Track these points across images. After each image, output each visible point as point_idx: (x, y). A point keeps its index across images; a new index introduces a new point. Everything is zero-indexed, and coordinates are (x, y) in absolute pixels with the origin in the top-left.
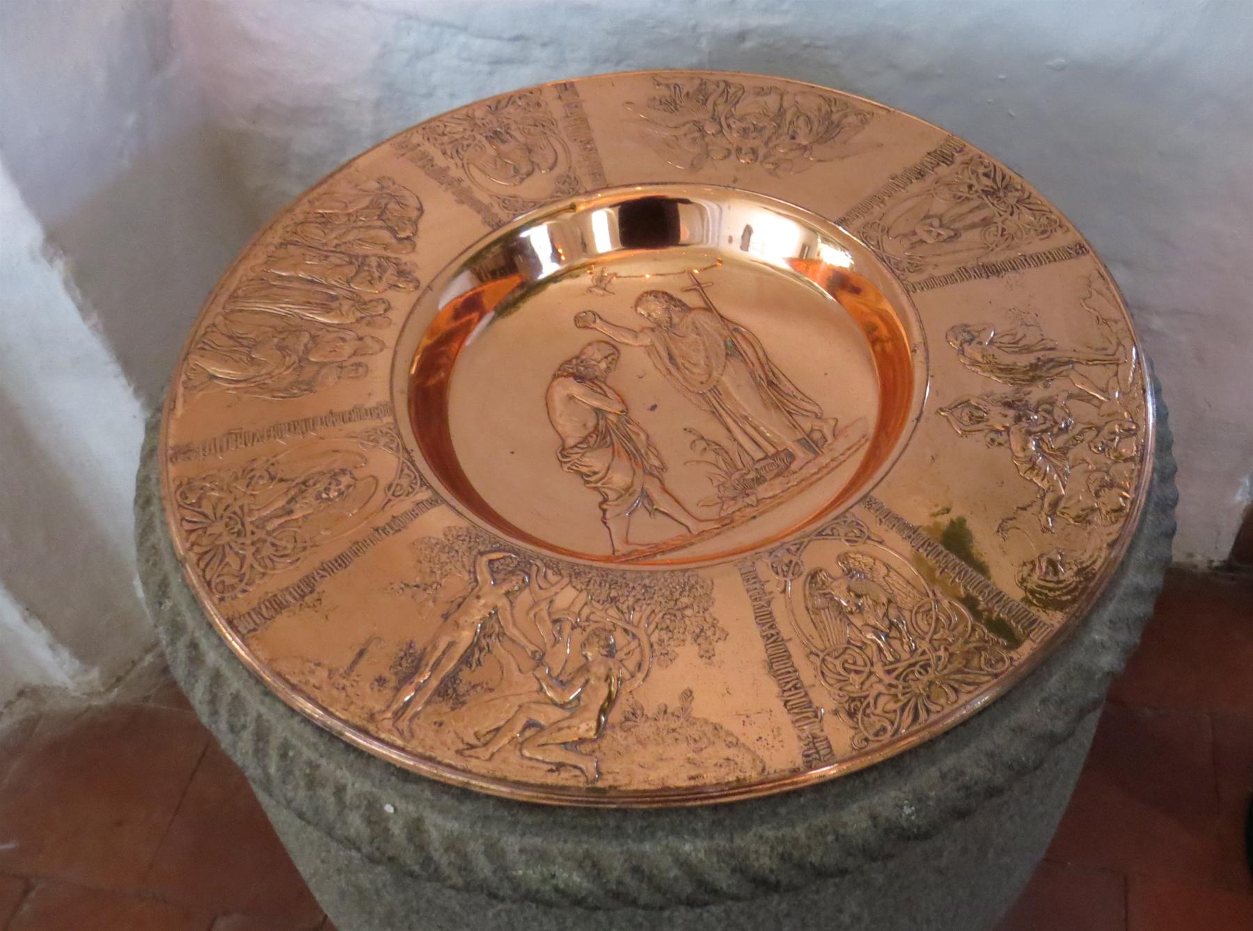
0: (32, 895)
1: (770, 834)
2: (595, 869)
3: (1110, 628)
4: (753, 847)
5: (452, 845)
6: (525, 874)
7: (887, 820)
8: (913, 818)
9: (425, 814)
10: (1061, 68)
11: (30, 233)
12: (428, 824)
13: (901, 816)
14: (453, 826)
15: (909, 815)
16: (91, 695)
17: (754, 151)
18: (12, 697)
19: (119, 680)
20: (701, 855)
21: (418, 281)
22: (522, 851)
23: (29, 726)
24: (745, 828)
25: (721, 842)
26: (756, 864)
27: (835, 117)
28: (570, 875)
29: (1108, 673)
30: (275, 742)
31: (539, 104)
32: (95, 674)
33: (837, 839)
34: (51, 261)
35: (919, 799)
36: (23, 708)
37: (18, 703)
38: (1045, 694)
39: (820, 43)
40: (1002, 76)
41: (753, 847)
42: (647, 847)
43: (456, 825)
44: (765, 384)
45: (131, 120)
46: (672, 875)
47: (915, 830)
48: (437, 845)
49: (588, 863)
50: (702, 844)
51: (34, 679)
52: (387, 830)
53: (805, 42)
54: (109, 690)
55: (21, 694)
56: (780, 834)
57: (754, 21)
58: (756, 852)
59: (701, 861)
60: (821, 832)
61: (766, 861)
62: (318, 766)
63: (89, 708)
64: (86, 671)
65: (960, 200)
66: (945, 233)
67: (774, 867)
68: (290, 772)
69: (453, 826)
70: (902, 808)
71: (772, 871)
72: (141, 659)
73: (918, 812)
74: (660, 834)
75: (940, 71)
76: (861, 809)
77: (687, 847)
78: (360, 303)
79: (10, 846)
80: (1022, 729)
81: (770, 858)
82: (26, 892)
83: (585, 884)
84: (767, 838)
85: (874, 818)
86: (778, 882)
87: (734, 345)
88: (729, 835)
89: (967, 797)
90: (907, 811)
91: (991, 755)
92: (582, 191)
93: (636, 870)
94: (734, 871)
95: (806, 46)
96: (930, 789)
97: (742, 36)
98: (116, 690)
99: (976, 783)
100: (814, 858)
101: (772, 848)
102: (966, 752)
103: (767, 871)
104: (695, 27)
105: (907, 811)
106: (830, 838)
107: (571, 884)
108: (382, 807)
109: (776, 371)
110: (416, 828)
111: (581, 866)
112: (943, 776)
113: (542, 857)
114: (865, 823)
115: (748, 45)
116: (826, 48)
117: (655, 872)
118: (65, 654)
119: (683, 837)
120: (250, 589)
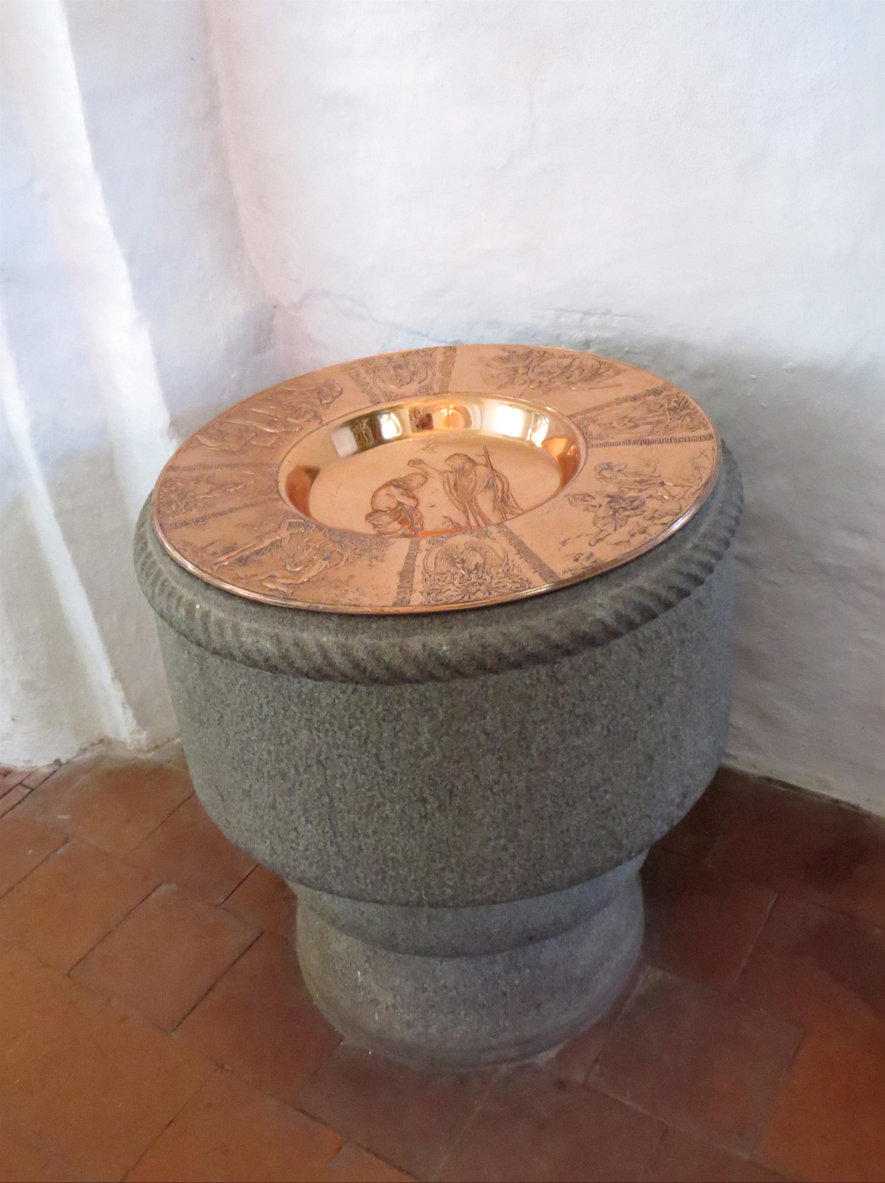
0: (67, 845)
1: (367, 641)
2: (277, 640)
3: (610, 600)
4: (357, 646)
5: (219, 623)
6: (246, 640)
7: (431, 648)
8: (447, 653)
9: (212, 610)
10: (793, 370)
11: (163, 419)
12: (212, 613)
13: (440, 650)
14: (222, 615)
15: (445, 651)
16: (140, 751)
17: (541, 382)
18: (96, 741)
19: (157, 747)
20: (330, 644)
21: (322, 421)
22: (248, 629)
23: (99, 759)
24: (354, 633)
25: (341, 639)
26: (355, 654)
27: (601, 371)
28: (266, 643)
29: (599, 620)
30: (162, 579)
31: (431, 355)
32: (143, 736)
33: (400, 650)
34: (171, 439)
35: (454, 643)
36: (100, 748)
37: (98, 746)
38: (550, 617)
39: (636, 350)
40: (754, 376)
41: (357, 646)
42: (305, 635)
43: (224, 615)
44: (499, 500)
45: (234, 375)
46: (313, 650)
47: (447, 661)
48: (212, 624)
49: (275, 638)
50: (332, 639)
51: (110, 733)
52: (194, 615)
53: (626, 349)
54: (149, 751)
55: (101, 741)
56: (372, 642)
57: (593, 334)
58: (357, 648)
59: (329, 647)
60: (394, 646)
61: (361, 654)
62: (176, 589)
63: (136, 758)
64: (139, 732)
65: (650, 411)
66: (629, 425)
67: (365, 658)
68: (163, 591)
69: (222, 615)
70: (442, 646)
71: (363, 659)
72: (173, 739)
73: (451, 650)
74: (312, 627)
75: (712, 371)
76: (419, 640)
77: (325, 639)
78: (287, 425)
79: (66, 817)
80: (527, 627)
81: (363, 653)
82: (65, 843)
83: (272, 649)
84: (365, 643)
85: (424, 645)
86: (366, 668)
87: (493, 483)
88: (345, 637)
89: (484, 653)
90: (445, 648)
91: (504, 634)
92: (432, 393)
93: (296, 644)
94: (343, 654)
95: (628, 352)
96: (461, 641)
97: (587, 344)
98: (153, 752)
99: (489, 645)
100: (387, 659)
101: (366, 647)
102: (490, 629)
103: (360, 659)
104: (558, 336)
105: (445, 648)
106: (397, 649)
107: (265, 647)
108: (195, 606)
109: (510, 495)
110: (206, 615)
111: (271, 638)
112: (471, 637)
113: (256, 633)
114: (419, 647)
115: (591, 350)
116: (640, 353)
117: (305, 647)
118: (130, 713)
119: (323, 632)
120: (176, 517)
